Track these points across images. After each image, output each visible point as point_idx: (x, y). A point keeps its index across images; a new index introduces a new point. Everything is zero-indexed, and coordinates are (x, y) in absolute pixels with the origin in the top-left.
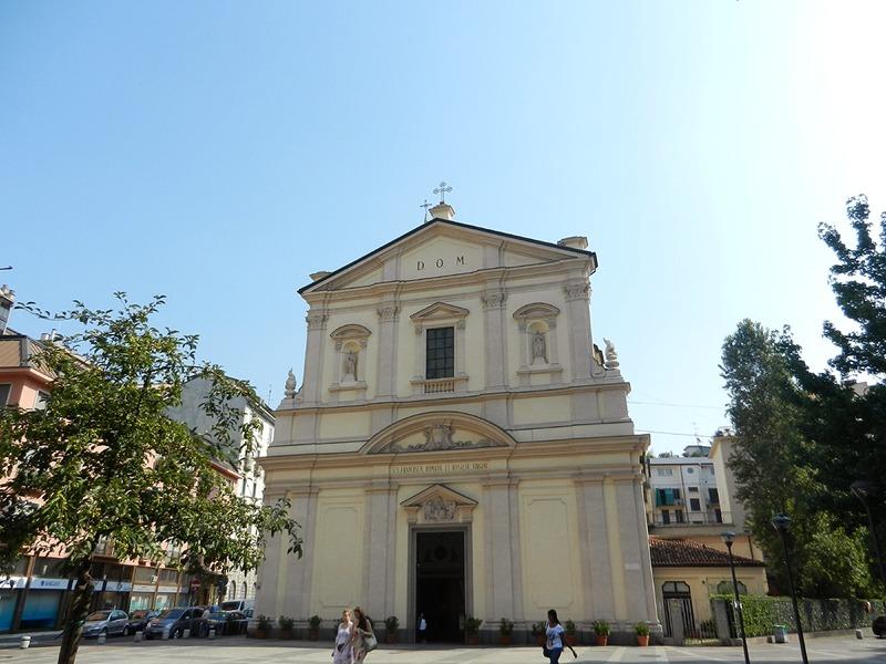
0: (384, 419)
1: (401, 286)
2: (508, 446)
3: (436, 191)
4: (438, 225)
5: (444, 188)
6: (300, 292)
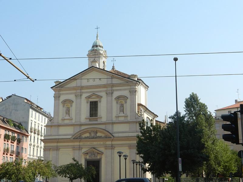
0: (77, 129)
1: (82, 88)
6: (51, 88)
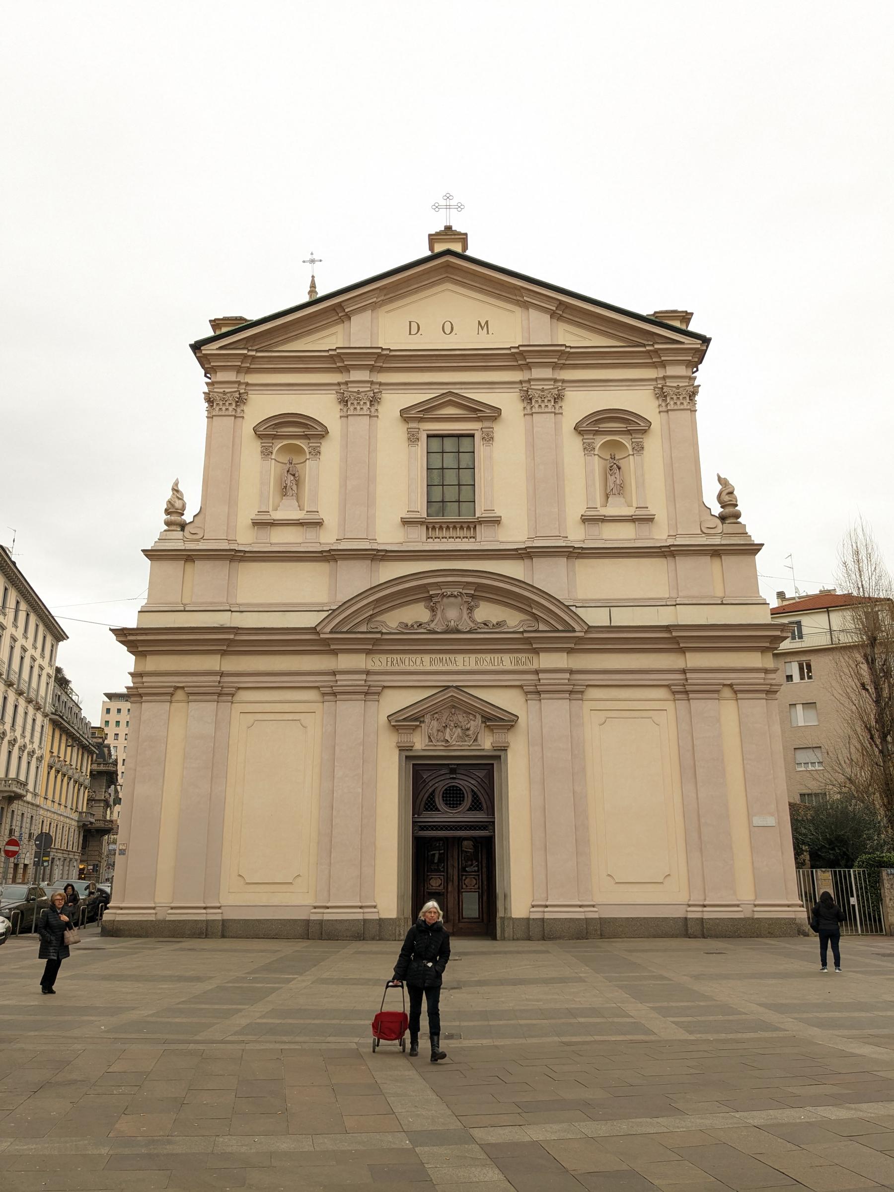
0: (356, 580)
1: (382, 359)
2: (574, 631)
3: (436, 207)
4: (448, 262)
5: (448, 203)
